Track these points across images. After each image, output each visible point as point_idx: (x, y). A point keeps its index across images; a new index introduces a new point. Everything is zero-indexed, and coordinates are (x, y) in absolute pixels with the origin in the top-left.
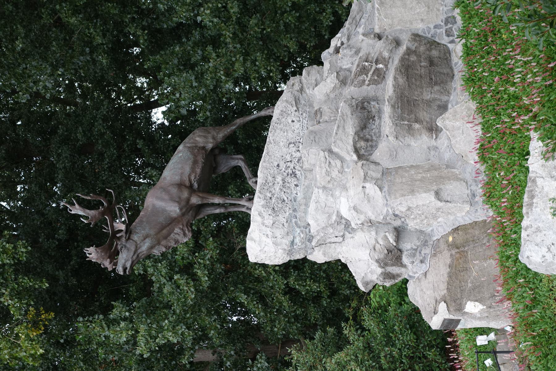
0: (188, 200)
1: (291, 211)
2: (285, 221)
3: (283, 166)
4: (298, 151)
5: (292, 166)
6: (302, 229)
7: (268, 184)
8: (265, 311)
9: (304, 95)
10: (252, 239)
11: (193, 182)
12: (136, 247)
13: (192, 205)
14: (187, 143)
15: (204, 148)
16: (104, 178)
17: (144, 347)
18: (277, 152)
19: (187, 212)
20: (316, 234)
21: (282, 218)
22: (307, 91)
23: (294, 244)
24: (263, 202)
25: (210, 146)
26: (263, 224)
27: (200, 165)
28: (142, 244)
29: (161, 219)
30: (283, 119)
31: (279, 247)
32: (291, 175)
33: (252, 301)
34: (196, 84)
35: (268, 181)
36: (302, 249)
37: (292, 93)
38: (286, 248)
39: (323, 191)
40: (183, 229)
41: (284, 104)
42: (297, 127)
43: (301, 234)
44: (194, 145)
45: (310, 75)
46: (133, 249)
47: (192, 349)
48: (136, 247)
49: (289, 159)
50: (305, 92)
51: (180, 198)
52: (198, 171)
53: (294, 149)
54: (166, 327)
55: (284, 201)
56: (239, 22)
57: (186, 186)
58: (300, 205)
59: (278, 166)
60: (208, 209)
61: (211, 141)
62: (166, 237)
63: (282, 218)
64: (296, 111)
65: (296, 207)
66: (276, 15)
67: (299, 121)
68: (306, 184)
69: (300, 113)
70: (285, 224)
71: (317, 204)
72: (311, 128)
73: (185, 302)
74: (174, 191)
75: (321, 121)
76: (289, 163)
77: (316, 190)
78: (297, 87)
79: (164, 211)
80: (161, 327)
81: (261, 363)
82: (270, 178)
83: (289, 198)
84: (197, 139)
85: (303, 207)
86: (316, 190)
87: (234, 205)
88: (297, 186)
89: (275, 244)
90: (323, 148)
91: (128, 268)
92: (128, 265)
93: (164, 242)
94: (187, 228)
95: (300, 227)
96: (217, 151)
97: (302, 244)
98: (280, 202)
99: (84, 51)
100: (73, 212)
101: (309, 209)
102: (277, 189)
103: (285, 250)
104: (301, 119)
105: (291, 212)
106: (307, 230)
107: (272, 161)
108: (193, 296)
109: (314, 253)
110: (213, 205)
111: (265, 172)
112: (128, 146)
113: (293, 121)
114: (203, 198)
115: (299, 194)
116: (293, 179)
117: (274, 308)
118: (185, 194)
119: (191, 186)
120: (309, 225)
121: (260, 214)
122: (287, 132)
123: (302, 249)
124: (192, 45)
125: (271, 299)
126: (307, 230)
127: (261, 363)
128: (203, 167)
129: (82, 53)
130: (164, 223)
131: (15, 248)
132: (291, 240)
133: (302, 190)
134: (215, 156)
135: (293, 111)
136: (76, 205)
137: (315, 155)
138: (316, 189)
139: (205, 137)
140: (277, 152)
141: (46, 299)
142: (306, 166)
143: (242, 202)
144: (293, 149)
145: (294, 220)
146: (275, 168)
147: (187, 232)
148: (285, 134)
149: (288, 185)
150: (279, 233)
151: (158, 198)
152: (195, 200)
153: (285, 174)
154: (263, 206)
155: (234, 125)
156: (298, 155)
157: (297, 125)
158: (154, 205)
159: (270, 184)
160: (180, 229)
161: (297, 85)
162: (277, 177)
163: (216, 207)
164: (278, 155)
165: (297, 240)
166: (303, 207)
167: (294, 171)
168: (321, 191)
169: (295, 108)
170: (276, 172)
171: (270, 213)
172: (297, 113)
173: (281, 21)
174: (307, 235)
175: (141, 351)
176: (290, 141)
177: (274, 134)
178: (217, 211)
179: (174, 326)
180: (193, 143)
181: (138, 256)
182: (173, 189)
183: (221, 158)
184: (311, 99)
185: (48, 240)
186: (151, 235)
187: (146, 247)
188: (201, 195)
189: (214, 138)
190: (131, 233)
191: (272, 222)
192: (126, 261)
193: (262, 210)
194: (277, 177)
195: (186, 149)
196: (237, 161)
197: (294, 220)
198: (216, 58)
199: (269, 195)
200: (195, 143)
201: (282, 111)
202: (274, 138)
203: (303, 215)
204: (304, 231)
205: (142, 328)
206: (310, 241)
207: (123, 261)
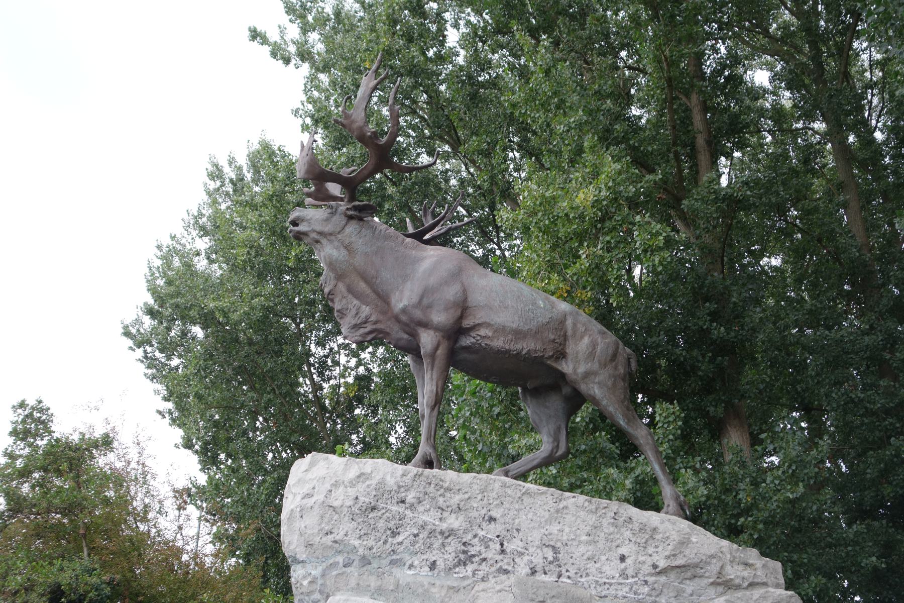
0: (426, 325)
2: (337, 538)
3: (490, 531)
4: (534, 572)
6: (320, 582)
7: (442, 495)
9: (712, 591)
11: (473, 334)
12: (331, 234)
16: (834, 395)
21: (345, 528)
24: (391, 482)
25: (566, 367)
26: (336, 485)
28: (336, 243)
29: (386, 276)
30: (628, 534)
32: (464, 552)
35: (448, 495)
40: (366, 322)
41: (675, 536)
42: (606, 568)
44: (570, 333)
46: (327, 229)
48: (331, 234)
49: (508, 547)
52: (498, 343)
53: (538, 561)
55: (394, 534)
57: (461, 318)
58: (380, 576)
59: (492, 519)
61: (581, 369)
63: (345, 528)
64: (655, 566)
65: (375, 565)
67: (623, 574)
68: (434, 590)
70: (330, 537)
74: (451, 293)
76: (498, 547)
78: (734, 572)
79: (405, 278)
82: (456, 499)
83: (402, 548)
84: (586, 340)
85: (373, 582)
88: (433, 566)
94: (370, 332)
96: (566, 390)
98: (391, 525)
102: (425, 518)
104: (630, 580)
105: (361, 551)
110: (424, 383)
111: (475, 487)
112: (891, 424)
115: (409, 572)
116: (451, 557)
118: (440, 317)
121: (362, 476)
122: (588, 543)
130: (379, 280)
131: (660, 249)
133: (420, 579)
135: (655, 558)
140: (530, 516)
145: (340, 559)
146: (484, 512)
147: (362, 331)
148: (584, 538)
149: (437, 544)
153: (468, 538)
154: (382, 482)
159: (441, 499)
161: (745, 574)
162: (461, 518)
164: (523, 520)
166: (373, 582)
167: (476, 559)
169: (662, 564)
170: (475, 514)
171: (362, 499)
172: (646, 569)
185: (708, 315)
189: (587, 375)
190: (361, 219)
191: (336, 504)
193: (373, 482)
194: (461, 518)
197: (340, 559)
199: (410, 497)
200: (574, 334)
202: (572, 509)
203: (353, 583)
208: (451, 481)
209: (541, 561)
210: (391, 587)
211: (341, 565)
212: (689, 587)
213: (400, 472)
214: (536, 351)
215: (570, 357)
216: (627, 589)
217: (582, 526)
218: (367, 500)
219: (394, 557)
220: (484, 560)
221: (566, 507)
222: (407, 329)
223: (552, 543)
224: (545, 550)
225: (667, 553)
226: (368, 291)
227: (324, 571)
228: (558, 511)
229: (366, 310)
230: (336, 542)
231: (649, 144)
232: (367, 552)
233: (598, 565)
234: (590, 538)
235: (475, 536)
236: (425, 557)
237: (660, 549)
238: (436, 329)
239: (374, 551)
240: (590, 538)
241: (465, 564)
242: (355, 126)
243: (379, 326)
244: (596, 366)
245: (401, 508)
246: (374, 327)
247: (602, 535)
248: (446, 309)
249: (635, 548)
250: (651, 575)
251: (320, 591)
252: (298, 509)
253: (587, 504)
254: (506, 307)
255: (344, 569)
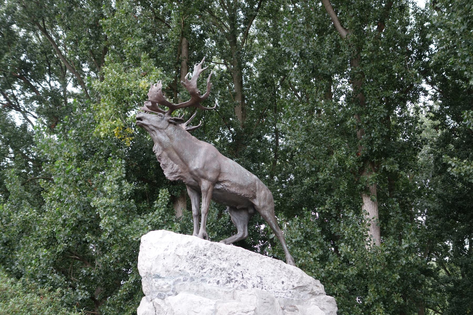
0: (205, 178)
1: (189, 277)
2: (181, 269)
3: (238, 269)
5: (239, 278)
6: (172, 287)
8: (122, 299)
9: (309, 296)
10: (164, 235)
11: (222, 184)
12: (161, 129)
13: (200, 181)
14: (259, 182)
15: (255, 197)
17: (99, 203)
18: (252, 264)
19: (194, 177)
20: (167, 302)
21: (184, 265)
22: (313, 299)
23: (156, 279)
24: (201, 247)
25: (256, 202)
26: (179, 246)
27: (239, 192)
28: (164, 134)
29: (187, 153)
31: (154, 262)
32: (229, 277)
33: (129, 287)
34: (293, 242)
35: (222, 253)
36: (151, 288)
37: (310, 283)
38: (153, 270)
39: (212, 310)
40: (176, 172)
41: (299, 275)
42: (277, 286)
43: (167, 286)
44: (257, 188)
45: (328, 303)
46: (159, 126)
47: (96, 241)
48: (161, 129)
49: (245, 276)
50: (311, 297)
51: (207, 170)
52: (233, 190)
53: (255, 283)
54: (111, 218)
55: (203, 269)
56: (340, 277)
57: (218, 177)
58: (198, 286)
59: (239, 265)
60: (196, 199)
61: (262, 204)
62: (169, 156)
63: (184, 265)
64: (293, 286)
65: (196, 281)
66: (347, 306)
67: (283, 289)
69: (292, 291)
70: (178, 268)
71: (198, 303)
72: (277, 300)
73: (131, 234)
74: (214, 166)
75: (285, 310)
77: (213, 302)
78: (316, 289)
79: (195, 156)
80: (112, 215)
81: (82, 294)
82: (225, 256)
83: (205, 275)
84: (263, 192)
85: (195, 288)
86: (213, 302)
87: (199, 225)
88: (218, 282)
89: (157, 258)
90: (258, 311)
91: (142, 122)
92: (144, 122)
93: (165, 154)
94: (178, 177)
95: (174, 284)
96: (251, 211)
97: (156, 287)
98: (201, 264)
99: (313, 166)
100: (195, 67)
101: (193, 295)
103: (151, 269)
105: (191, 275)
106: (170, 293)
107: (243, 259)
108: (134, 239)
109: (147, 303)
110: (200, 201)
111: (232, 251)
113: (283, 283)
114: (207, 192)
115: (210, 285)
117: (123, 306)
118: (210, 175)
119: (218, 182)
120: (177, 294)
122: (272, 276)
123: (151, 288)
124: (321, 242)
125: (131, 303)
126: (170, 293)
127: (82, 294)
128: (236, 194)
129: (311, 166)
132: (161, 275)
134: (246, 209)
136: (202, 70)
137: (250, 302)
138: (214, 303)
139: (265, 199)
140: (252, 264)
141: (141, 146)
142: (238, 293)
143: (202, 231)
144: (256, 281)
145: (181, 278)
146: (236, 261)
147: (174, 176)
148: (271, 274)
149: (219, 274)
150: (169, 262)
151: (206, 154)
152: (205, 185)
153: (230, 272)
154: (197, 246)
155: (276, 227)
156: (250, 286)
157: (280, 286)
158: (201, 147)
159: (220, 255)
160: (177, 170)
162: (227, 263)
163: (198, 207)
165: (160, 282)
166: (195, 288)
167: (233, 281)
168: (212, 307)
169: (296, 285)
170: (232, 262)
171: (190, 253)
172: (291, 287)
173: (342, 310)
174: (166, 292)
175: (96, 201)
176: (264, 278)
177: (270, 262)
178: (194, 208)
179: (112, 224)
180: (259, 188)
181: (153, 130)
182: (216, 165)
183: (244, 216)
184: (304, 303)
186: (172, 142)
187: (161, 137)
188: (210, 190)
189: (264, 207)
190: (175, 124)
191: (180, 254)
192: (149, 120)
193: (194, 246)
194: (227, 263)
195: (253, 181)
196: (242, 230)
197: (181, 278)
198: (314, 257)
199: (209, 254)
200: (259, 189)
201: (292, 272)
202: (266, 262)
203: (187, 288)
204: (169, 289)
205: (113, 201)
206: (160, 296)
207: (149, 118)
208: (224, 248)
209: (256, 282)
210: (202, 291)
211: (182, 280)
212: (302, 294)
213: (205, 243)
214: (247, 195)
215: (257, 198)
216: (284, 294)
217: (270, 270)
218: (192, 254)
219: (203, 278)
220: (237, 281)
221: (264, 262)
222: (195, 178)
223: (260, 275)
224: (258, 278)
225: (297, 281)
226: (178, 158)
227: (174, 282)
228: (261, 263)
229: (176, 167)
230: (180, 271)
231: (167, 61)
232: (193, 276)
233: (275, 285)
234: (272, 274)
235: (232, 271)
236: (214, 279)
237: (294, 279)
238: (209, 180)
239: (195, 275)
240: (272, 274)
241: (230, 282)
242: (191, 87)
243: (182, 174)
244: (267, 204)
245: (203, 258)
246: (180, 175)
247: (276, 273)
248: (213, 172)
249: (287, 278)
250: (292, 289)
251: (172, 291)
252: (163, 255)
253: (271, 261)
254: (237, 175)
255: (184, 282)
